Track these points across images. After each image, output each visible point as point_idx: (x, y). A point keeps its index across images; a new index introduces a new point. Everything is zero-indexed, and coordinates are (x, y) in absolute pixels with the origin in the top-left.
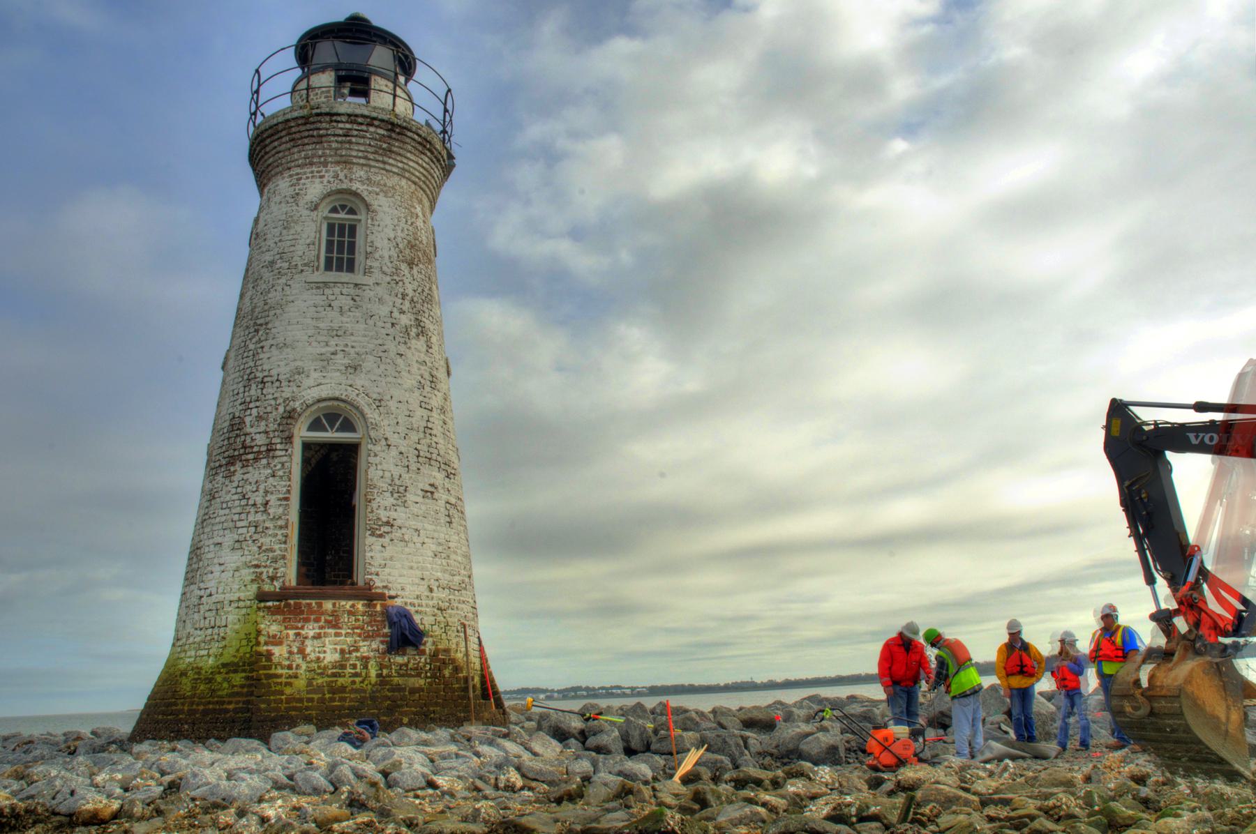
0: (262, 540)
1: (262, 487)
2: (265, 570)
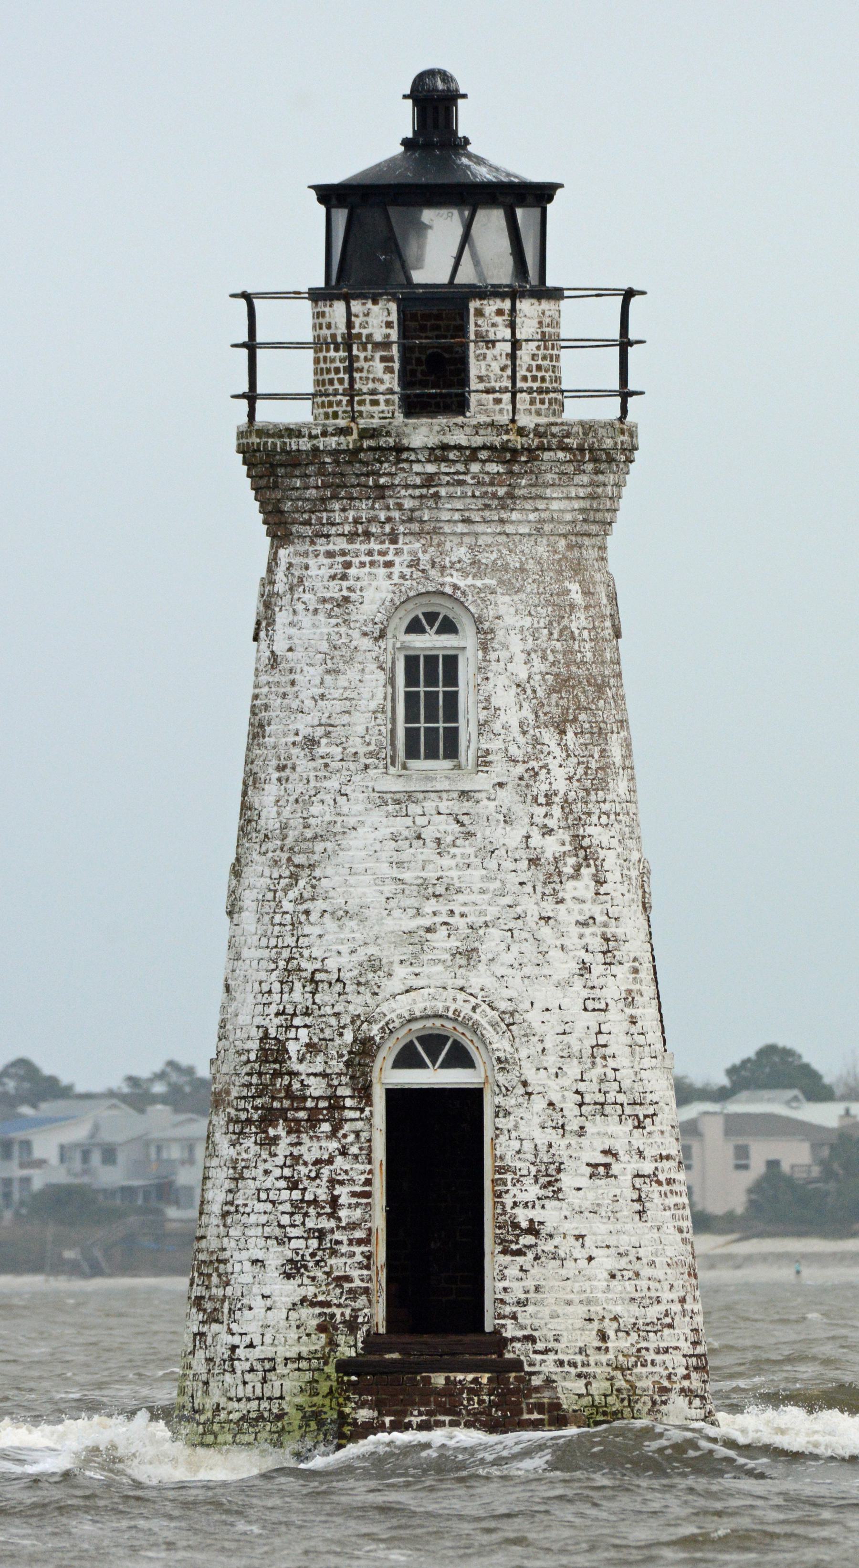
0: (332, 1261)
1: (326, 1171)
2: (338, 1312)
